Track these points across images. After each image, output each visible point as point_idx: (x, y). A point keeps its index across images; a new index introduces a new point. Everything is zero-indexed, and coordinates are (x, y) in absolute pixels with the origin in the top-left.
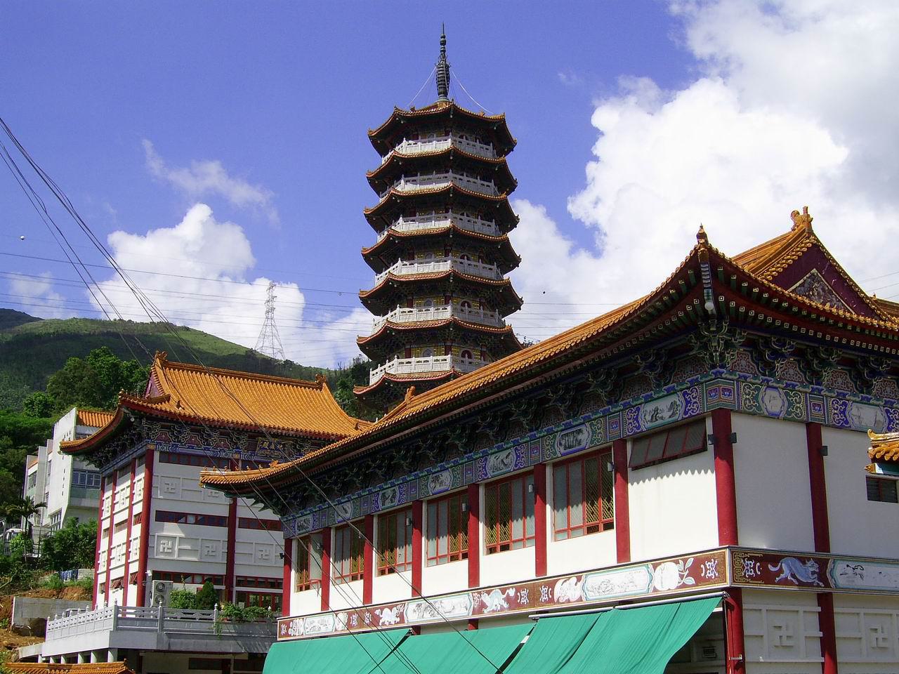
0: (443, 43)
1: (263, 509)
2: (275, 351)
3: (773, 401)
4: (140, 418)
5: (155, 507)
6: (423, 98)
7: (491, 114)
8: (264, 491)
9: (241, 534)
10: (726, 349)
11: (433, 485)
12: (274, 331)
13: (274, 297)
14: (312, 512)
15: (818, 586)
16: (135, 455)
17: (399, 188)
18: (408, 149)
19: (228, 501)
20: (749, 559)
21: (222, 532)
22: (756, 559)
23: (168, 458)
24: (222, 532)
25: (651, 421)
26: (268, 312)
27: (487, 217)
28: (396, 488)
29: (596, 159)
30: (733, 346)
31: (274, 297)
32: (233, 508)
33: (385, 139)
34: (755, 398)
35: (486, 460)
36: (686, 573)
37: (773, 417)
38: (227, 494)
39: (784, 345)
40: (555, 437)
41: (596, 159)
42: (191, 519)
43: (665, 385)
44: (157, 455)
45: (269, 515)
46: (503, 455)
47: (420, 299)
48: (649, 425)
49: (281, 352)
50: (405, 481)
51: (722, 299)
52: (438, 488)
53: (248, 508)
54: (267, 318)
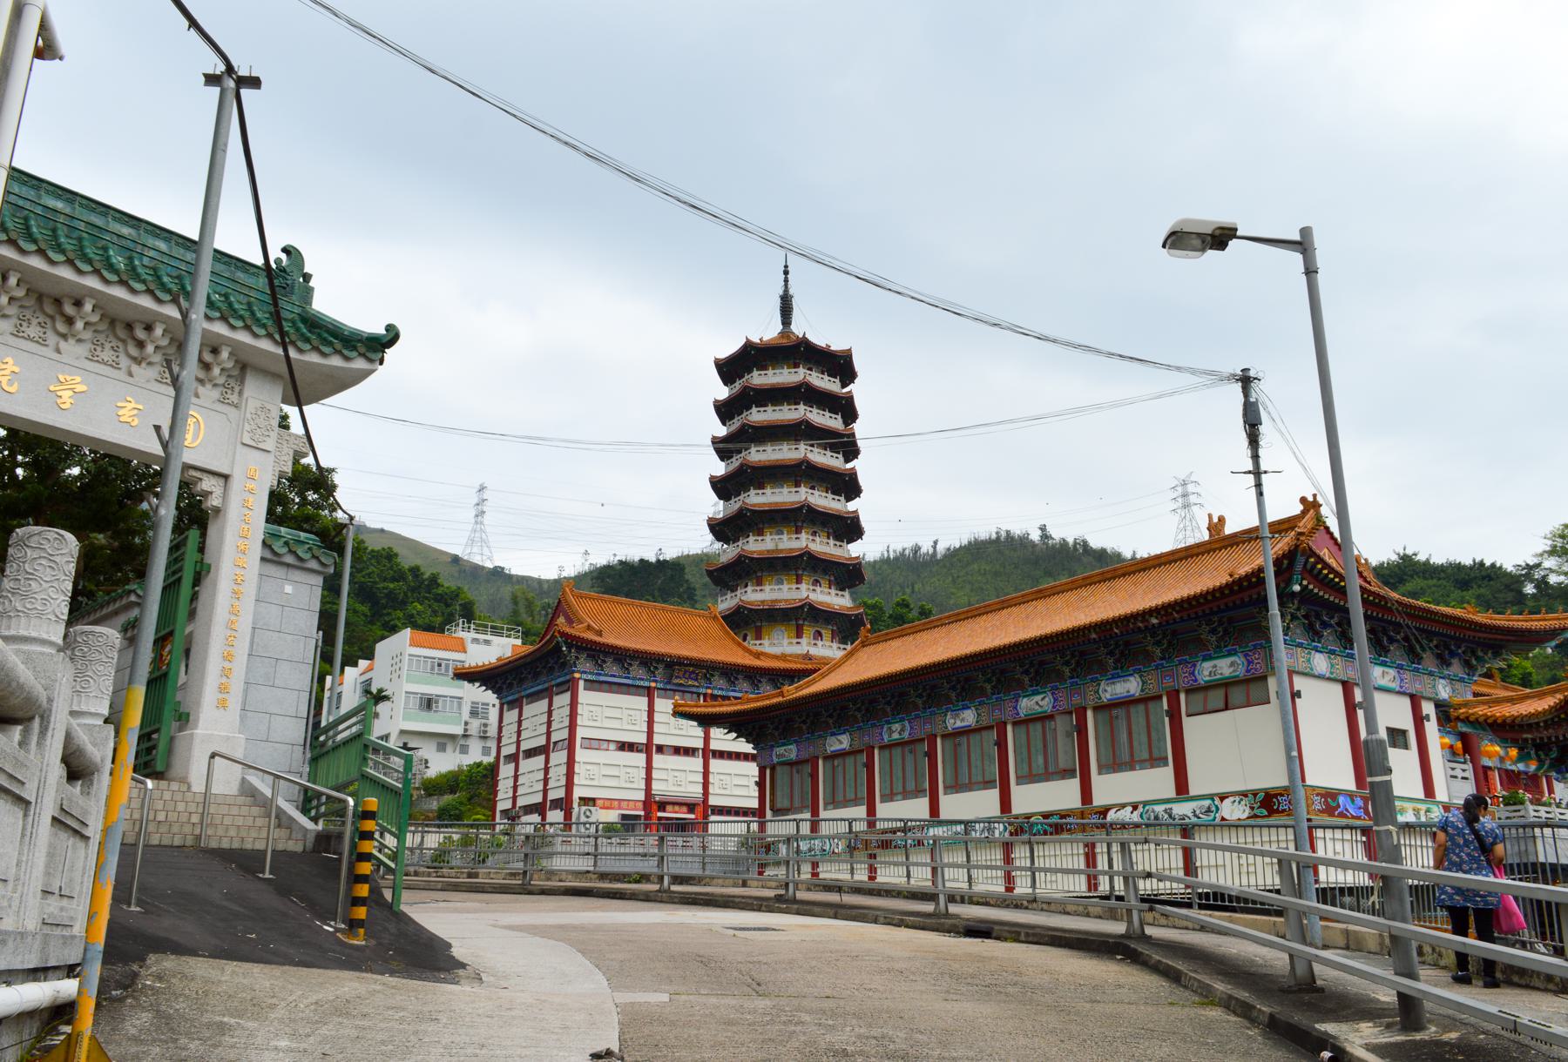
0: (786, 273)
1: (737, 737)
2: (484, 558)
3: (1320, 663)
4: (570, 647)
5: (581, 733)
6: (767, 330)
7: (837, 345)
8: (738, 723)
9: (658, 760)
10: (1291, 620)
11: (952, 721)
12: (484, 536)
13: (484, 500)
14: (796, 742)
15: (1364, 819)
17: (750, 418)
18: (760, 378)
19: (699, 732)
20: (1317, 795)
21: (641, 758)
23: (593, 685)
24: (641, 758)
25: (1210, 675)
26: (477, 516)
27: (834, 448)
28: (906, 723)
29: (1474, 561)
30: (1297, 618)
31: (484, 500)
32: (707, 739)
33: (729, 369)
34: (1309, 661)
35: (1017, 701)
36: (1256, 806)
37: (1320, 677)
38: (700, 724)
39: (1332, 618)
40: (1099, 685)
41: (1474, 561)
42: (612, 746)
43: (1225, 646)
44: (581, 683)
45: (746, 747)
46: (1038, 698)
47: (770, 527)
48: (1207, 678)
49: (490, 559)
51: (1305, 583)
52: (959, 724)
53: (722, 739)
54: (476, 523)
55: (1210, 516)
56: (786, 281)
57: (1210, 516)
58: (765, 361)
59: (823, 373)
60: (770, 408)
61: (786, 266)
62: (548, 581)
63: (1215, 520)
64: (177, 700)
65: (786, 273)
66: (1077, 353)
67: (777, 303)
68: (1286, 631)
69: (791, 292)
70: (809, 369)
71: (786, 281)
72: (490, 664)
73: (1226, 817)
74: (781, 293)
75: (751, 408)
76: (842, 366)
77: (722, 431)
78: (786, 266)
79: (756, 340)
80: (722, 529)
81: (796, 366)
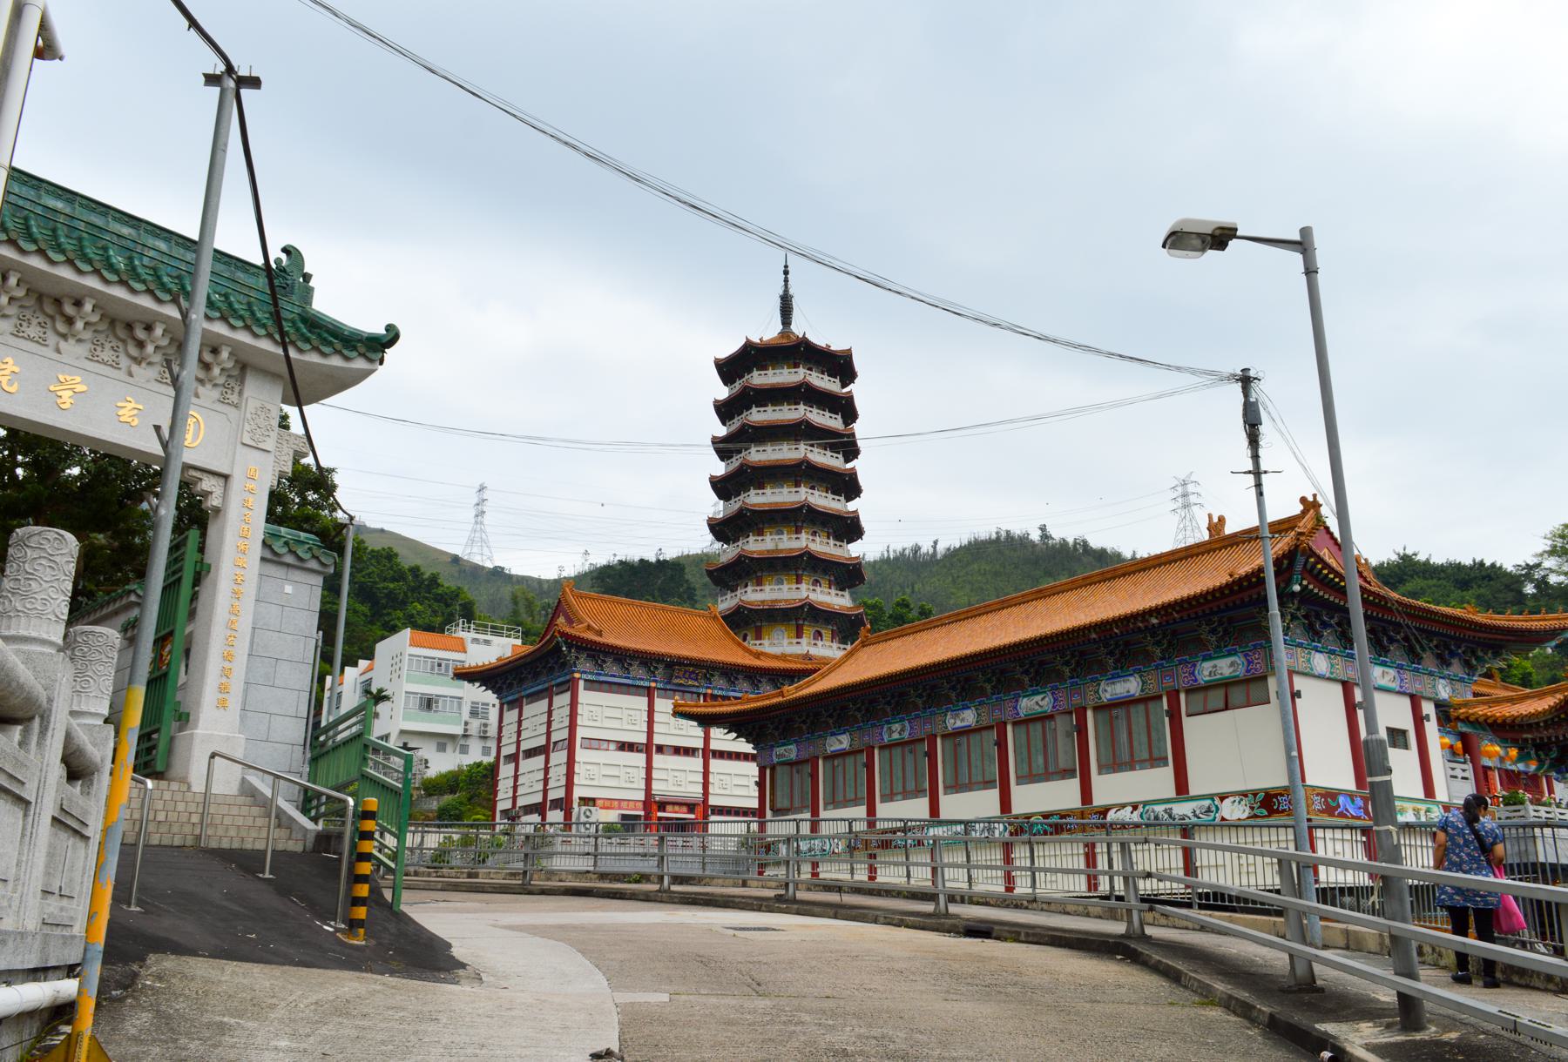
0: (786, 273)
1: (737, 737)
2: (484, 558)
3: (1320, 663)
5: (581, 733)
6: (767, 330)
7: (837, 345)
8: (738, 723)
9: (658, 760)
10: (1291, 620)
11: (952, 721)
13: (484, 500)
14: (796, 742)
15: (1364, 819)
16: (553, 683)
17: (750, 418)
18: (760, 378)
19: (699, 732)
20: (1317, 795)
21: (641, 758)
22: (1322, 795)
23: (593, 685)
24: (641, 758)
25: (1210, 675)
26: (477, 516)
27: (834, 448)
28: (906, 723)
29: (1474, 561)
30: (1297, 618)
31: (484, 500)
32: (707, 739)
33: (729, 369)
34: (1309, 661)
35: (1017, 701)
36: (1256, 806)
37: (1320, 677)
38: (700, 724)
41: (1474, 561)
42: (612, 746)
43: (1225, 646)
44: (581, 683)
45: (746, 747)
47: (770, 527)
48: (1207, 678)
49: (490, 559)
50: (917, 717)
51: (1305, 583)
52: (959, 724)
53: (722, 739)
54: (476, 523)
55: (1210, 516)
56: (786, 281)
57: (1210, 516)
58: (765, 361)
59: (823, 373)
60: (770, 408)
61: (786, 266)
62: (548, 581)
63: (1215, 520)
64: (177, 700)
65: (786, 273)
66: (1077, 353)
67: (777, 303)
68: (1286, 631)
69: (791, 292)
70: (809, 369)
71: (786, 281)
72: (490, 664)
73: (1226, 817)
74: (781, 293)
75: (751, 408)
76: (842, 366)
77: (722, 431)
78: (786, 266)
79: (756, 340)
80: (722, 529)
81: (796, 366)
